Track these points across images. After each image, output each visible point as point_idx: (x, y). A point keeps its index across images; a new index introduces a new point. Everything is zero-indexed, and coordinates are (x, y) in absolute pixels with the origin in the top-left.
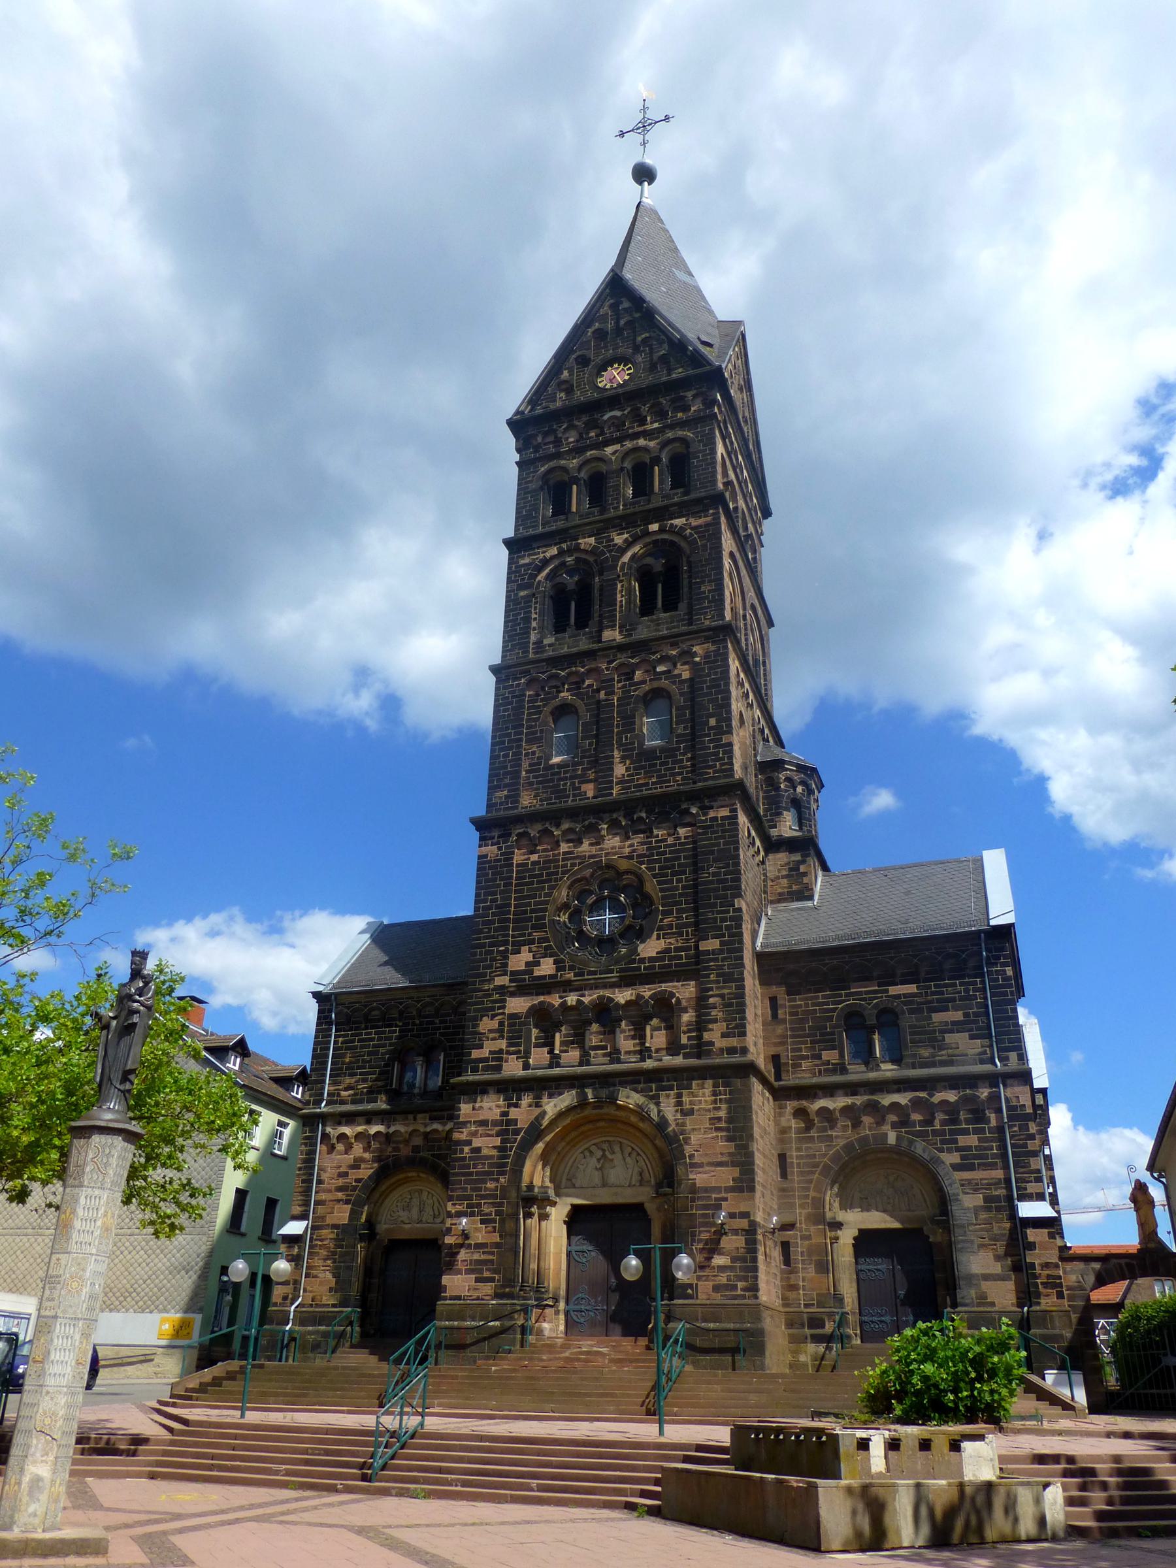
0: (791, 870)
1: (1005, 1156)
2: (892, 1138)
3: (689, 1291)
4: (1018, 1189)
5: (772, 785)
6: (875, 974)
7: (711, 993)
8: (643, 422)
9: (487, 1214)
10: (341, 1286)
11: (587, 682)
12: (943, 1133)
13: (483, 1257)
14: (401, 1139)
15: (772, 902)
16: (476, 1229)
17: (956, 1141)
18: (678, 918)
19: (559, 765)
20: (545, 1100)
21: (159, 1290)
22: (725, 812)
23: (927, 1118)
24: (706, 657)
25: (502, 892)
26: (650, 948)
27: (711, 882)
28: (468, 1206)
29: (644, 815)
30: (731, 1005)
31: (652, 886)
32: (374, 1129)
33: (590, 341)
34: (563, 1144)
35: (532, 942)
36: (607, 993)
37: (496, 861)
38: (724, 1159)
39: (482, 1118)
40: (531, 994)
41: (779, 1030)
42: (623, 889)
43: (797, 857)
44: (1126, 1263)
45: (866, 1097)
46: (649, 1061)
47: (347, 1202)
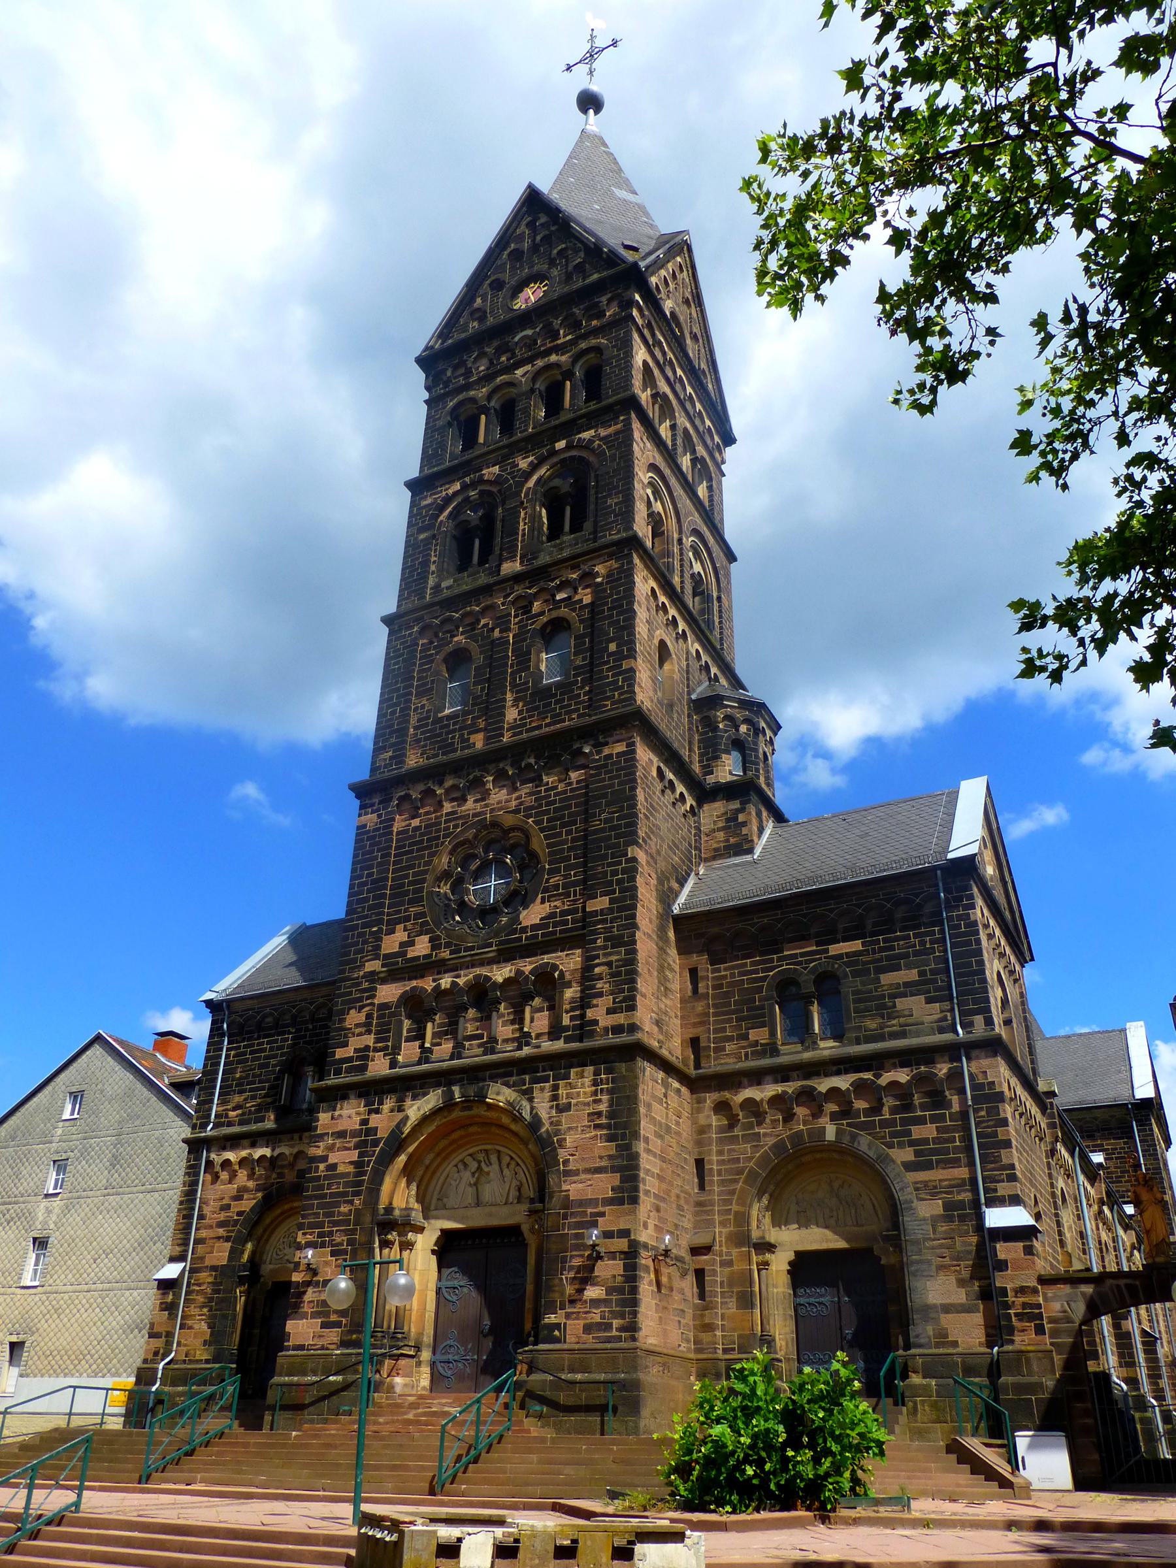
0: (728, 820)
1: (969, 1149)
2: (831, 1132)
3: (557, 1333)
4: (986, 1191)
5: (709, 725)
6: (813, 931)
8: (556, 336)
9: (337, 1245)
10: (216, 1337)
11: (483, 622)
14: (285, 1163)
15: (706, 860)
16: (327, 1263)
17: (909, 1133)
18: (565, 877)
19: (448, 717)
20: (408, 1102)
21: (113, 1351)
22: (620, 748)
23: (875, 1104)
24: (608, 576)
25: (379, 864)
26: (533, 914)
27: (603, 830)
29: (532, 761)
30: (618, 974)
31: (539, 843)
32: (258, 1153)
33: (505, 263)
34: (431, 1156)
35: (407, 919)
36: (483, 971)
38: (603, 1164)
39: (340, 1128)
40: (403, 979)
41: (700, 1007)
42: (510, 850)
43: (735, 805)
44: (1126, 1285)
45: (800, 1083)
46: (525, 1048)
47: (227, 1239)
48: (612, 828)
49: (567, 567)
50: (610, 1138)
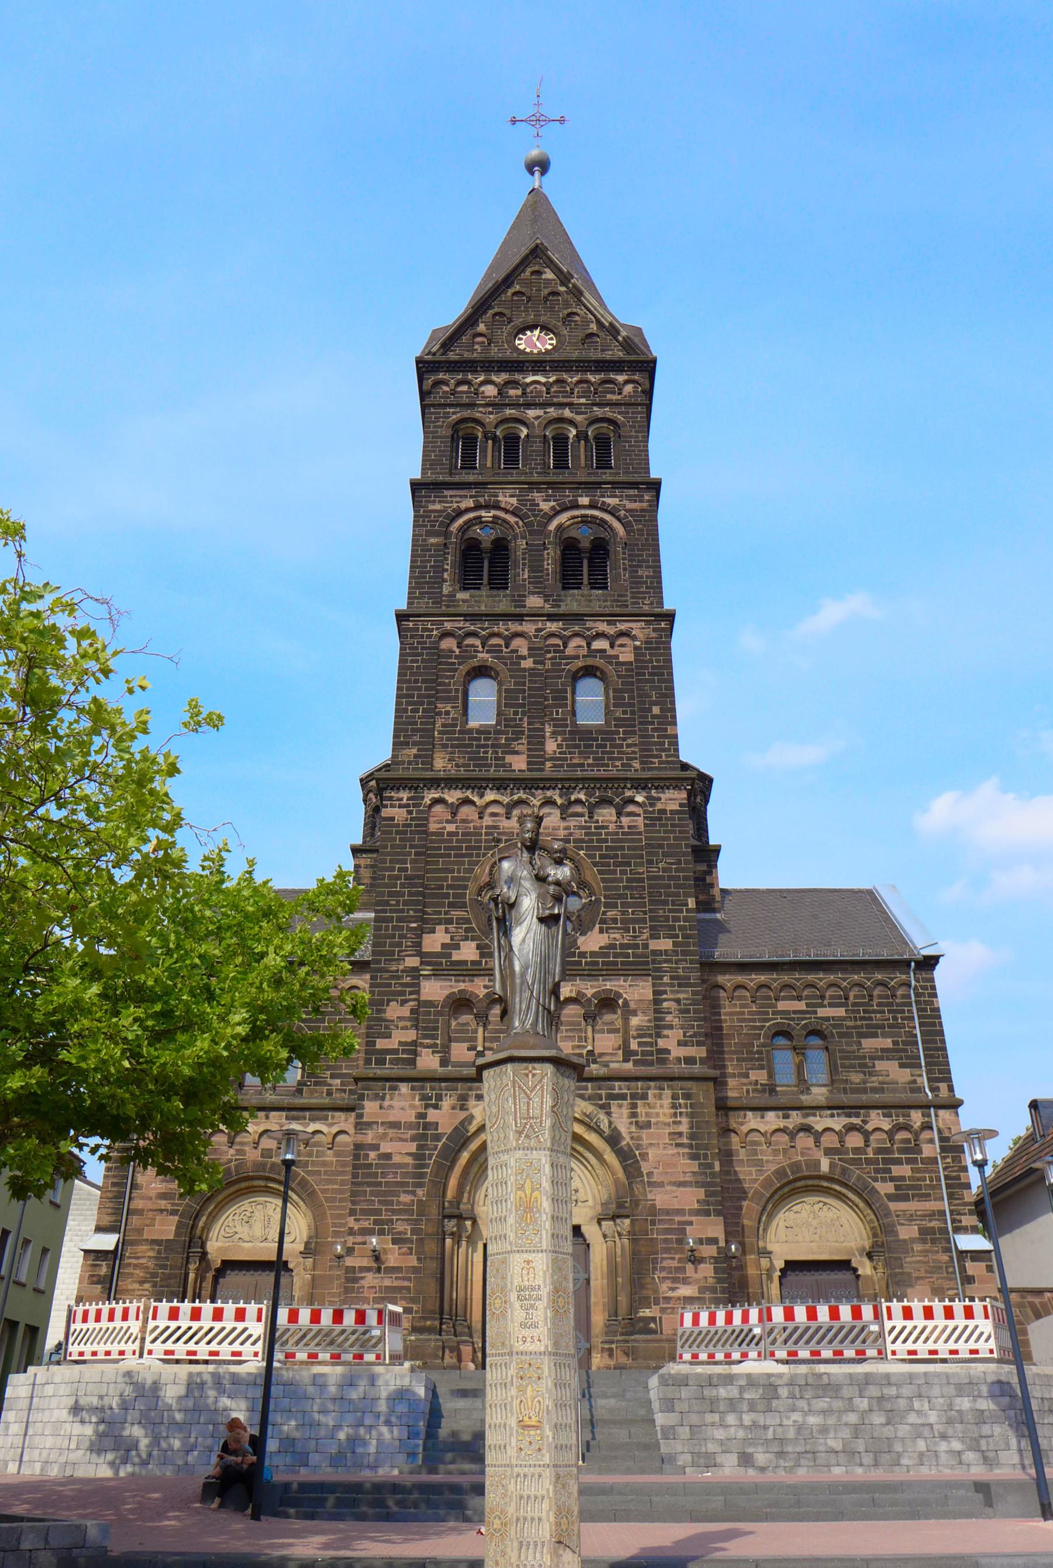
4: (953, 1221)
7: (665, 996)
9: (400, 1233)
12: (875, 1162)
13: (397, 1283)
17: (889, 1171)
18: (623, 913)
24: (646, 643)
27: (662, 878)
28: (376, 1222)
35: (449, 921)
37: (404, 825)
39: (391, 1119)
47: (173, 1213)
48: (670, 878)
49: (603, 621)
50: (694, 1157)
